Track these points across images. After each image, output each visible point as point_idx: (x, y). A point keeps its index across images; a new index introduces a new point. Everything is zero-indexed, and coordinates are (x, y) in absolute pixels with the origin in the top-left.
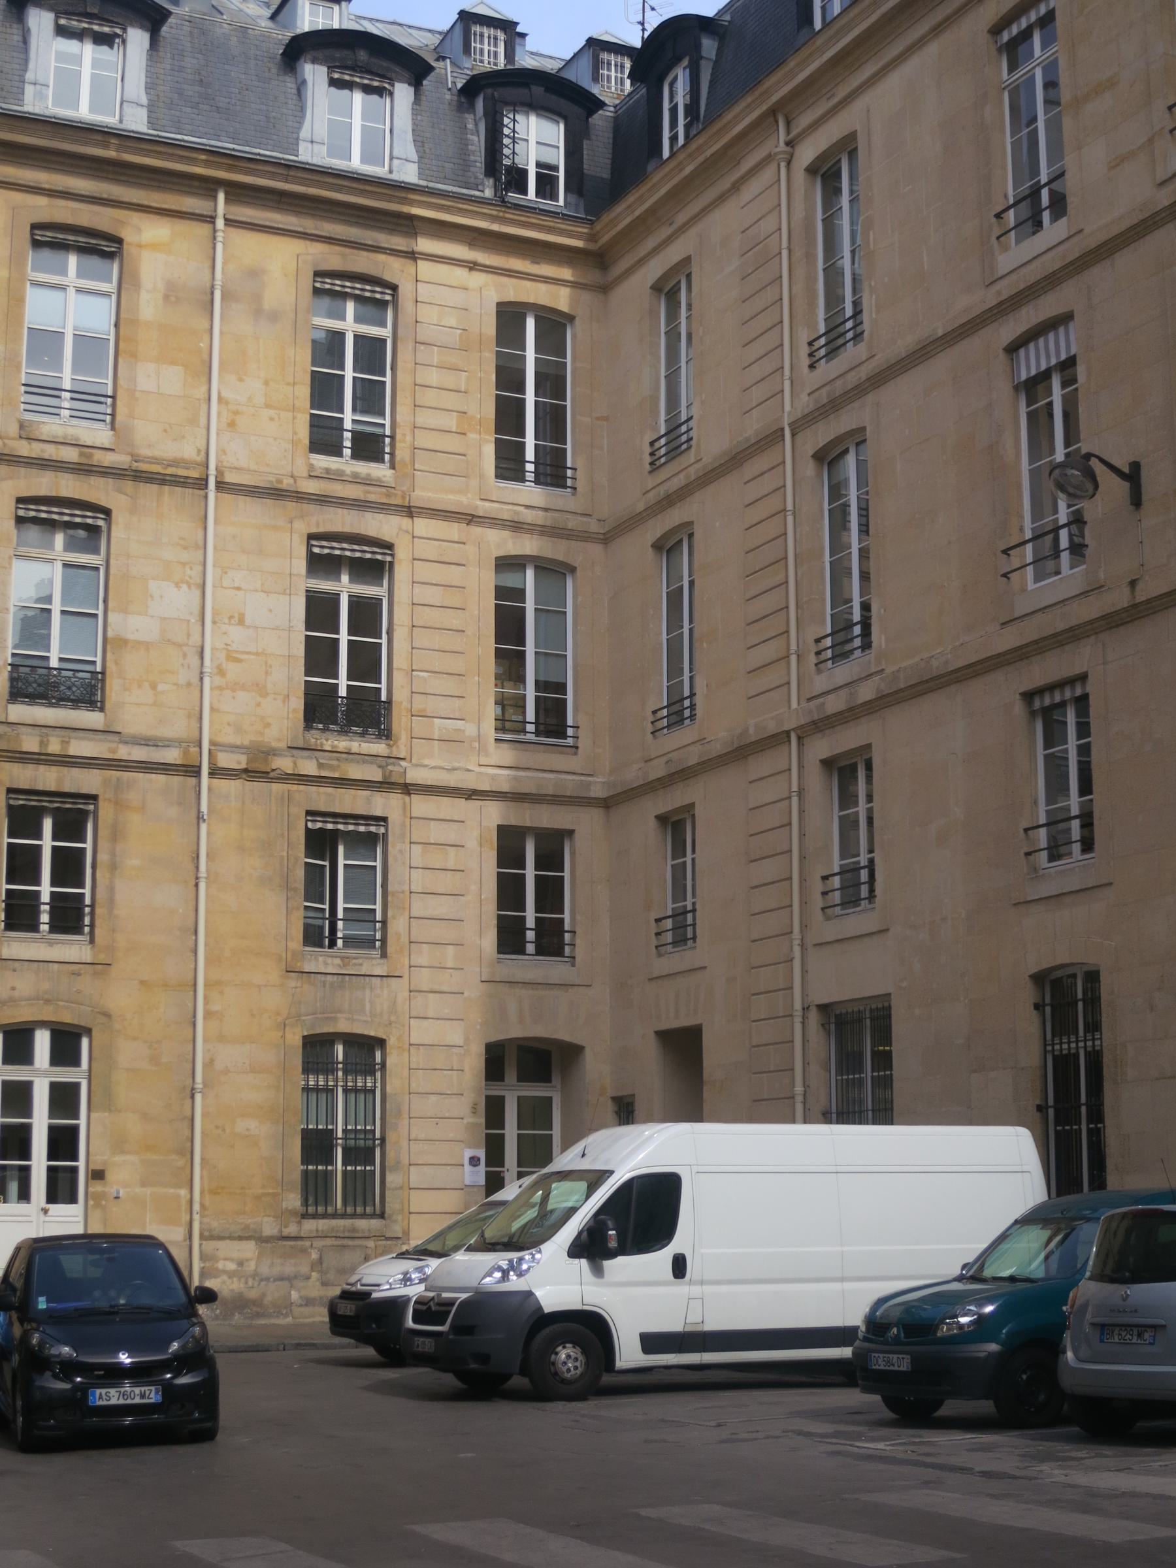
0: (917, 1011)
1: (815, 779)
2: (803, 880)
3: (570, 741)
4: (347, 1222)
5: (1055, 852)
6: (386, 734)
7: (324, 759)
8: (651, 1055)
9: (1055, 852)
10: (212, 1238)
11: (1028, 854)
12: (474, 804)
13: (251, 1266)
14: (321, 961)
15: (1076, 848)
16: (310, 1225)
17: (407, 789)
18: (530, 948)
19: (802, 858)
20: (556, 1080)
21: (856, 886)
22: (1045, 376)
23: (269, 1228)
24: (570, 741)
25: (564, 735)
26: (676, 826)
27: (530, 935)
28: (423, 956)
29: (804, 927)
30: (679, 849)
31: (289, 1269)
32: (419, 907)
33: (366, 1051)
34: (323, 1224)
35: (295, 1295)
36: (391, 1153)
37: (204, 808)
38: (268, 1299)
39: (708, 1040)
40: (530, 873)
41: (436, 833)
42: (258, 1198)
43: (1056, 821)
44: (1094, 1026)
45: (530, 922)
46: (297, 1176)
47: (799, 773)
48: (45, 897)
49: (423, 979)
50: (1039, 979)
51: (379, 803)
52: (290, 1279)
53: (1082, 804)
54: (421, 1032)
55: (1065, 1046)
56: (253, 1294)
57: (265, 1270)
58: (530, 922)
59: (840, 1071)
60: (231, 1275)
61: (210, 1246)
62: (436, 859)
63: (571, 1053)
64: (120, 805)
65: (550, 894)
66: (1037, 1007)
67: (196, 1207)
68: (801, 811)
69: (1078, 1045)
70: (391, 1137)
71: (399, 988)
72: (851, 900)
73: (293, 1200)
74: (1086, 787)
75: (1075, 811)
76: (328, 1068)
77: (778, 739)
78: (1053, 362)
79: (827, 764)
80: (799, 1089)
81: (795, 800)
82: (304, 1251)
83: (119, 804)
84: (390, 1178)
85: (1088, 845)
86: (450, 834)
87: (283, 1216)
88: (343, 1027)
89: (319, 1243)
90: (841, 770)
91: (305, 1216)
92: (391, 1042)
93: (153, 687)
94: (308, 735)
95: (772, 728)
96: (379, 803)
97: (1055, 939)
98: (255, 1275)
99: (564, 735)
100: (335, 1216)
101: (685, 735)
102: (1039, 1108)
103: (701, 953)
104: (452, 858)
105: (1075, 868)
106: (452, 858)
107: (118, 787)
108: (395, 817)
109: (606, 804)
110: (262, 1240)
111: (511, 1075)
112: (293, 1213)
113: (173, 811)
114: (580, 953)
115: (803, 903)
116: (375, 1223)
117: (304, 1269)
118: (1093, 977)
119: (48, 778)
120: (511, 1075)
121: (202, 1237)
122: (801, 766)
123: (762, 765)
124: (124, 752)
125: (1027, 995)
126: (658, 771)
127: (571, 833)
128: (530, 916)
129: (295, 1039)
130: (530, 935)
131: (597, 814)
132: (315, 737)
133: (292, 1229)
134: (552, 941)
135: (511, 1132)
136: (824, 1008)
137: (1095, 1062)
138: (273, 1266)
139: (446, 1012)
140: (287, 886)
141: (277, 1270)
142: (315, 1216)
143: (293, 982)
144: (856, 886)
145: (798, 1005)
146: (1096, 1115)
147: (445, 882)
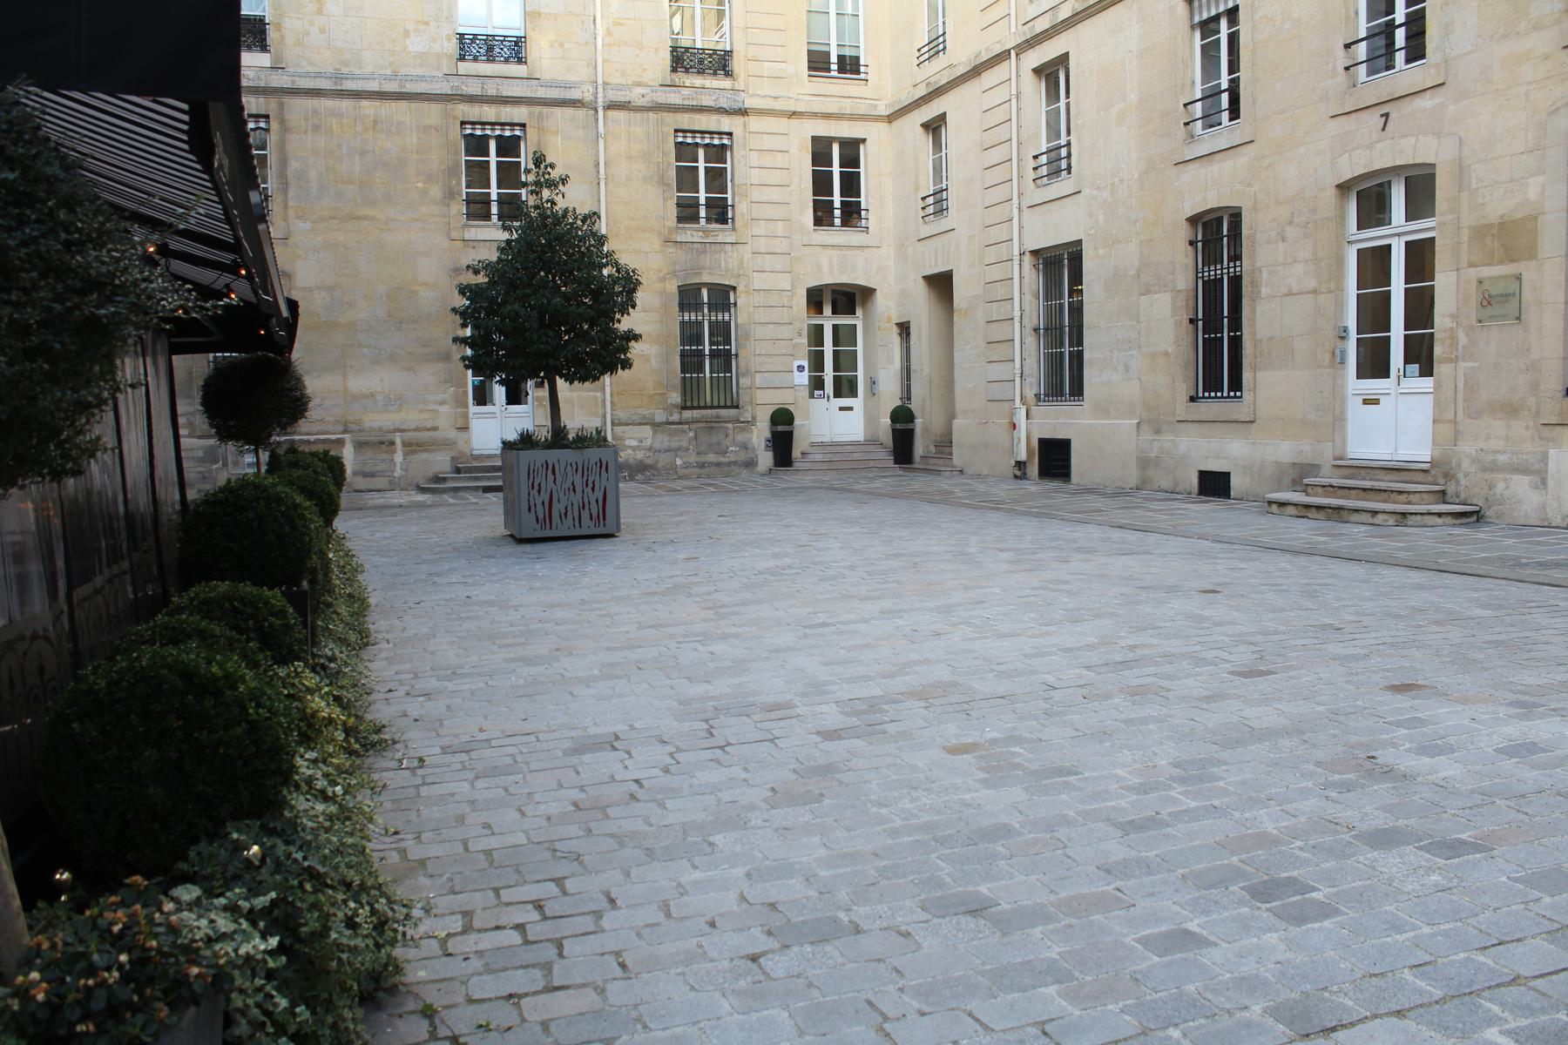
0: (1101, 251)
1: (1029, 79)
2: (1019, 160)
3: (862, 76)
4: (714, 411)
5: (1210, 120)
6: (728, 74)
7: (685, 92)
8: (921, 291)
9: (1210, 120)
10: (620, 424)
11: (1186, 124)
12: (794, 122)
13: (648, 442)
14: (690, 234)
15: (1225, 116)
16: (687, 414)
17: (743, 112)
18: (837, 221)
19: (1019, 144)
20: (859, 312)
21: (1056, 163)
22: (1216, 19)
23: (660, 416)
24: (862, 76)
25: (858, 72)
26: (934, 127)
27: (837, 213)
28: (760, 229)
29: (1020, 194)
30: (937, 145)
31: (674, 444)
32: (756, 194)
33: (722, 297)
34: (696, 413)
35: (679, 462)
36: (742, 364)
37: (601, 129)
38: (660, 465)
39: (957, 281)
40: (836, 170)
41: (768, 142)
42: (651, 397)
43: (1212, 95)
44: (1236, 257)
45: (837, 204)
46: (677, 381)
47: (1018, 82)
48: (494, 197)
49: (762, 245)
50: (1193, 221)
51: (725, 123)
52: (676, 451)
53: (1231, 81)
54: (759, 281)
55: (1211, 273)
56: (649, 462)
57: (657, 445)
58: (837, 204)
59: (1046, 299)
60: (634, 449)
61: (618, 429)
62: (768, 161)
63: (867, 293)
64: (541, 129)
65: (851, 184)
66: (1191, 243)
67: (608, 404)
68: (1019, 109)
69: (1224, 271)
70: (742, 354)
71: (745, 251)
72: (1055, 173)
73: (675, 397)
74: (1234, 66)
75: (1225, 86)
76: (697, 307)
77: (1003, 56)
78: (1222, 9)
79: (1037, 71)
80: (1017, 313)
81: (1014, 101)
82: (683, 431)
83: (540, 129)
84: (742, 381)
85: (1235, 112)
86: (778, 143)
87: (669, 409)
88: (706, 278)
89: (694, 426)
90: (1048, 77)
91: (684, 408)
92: (740, 288)
93: (561, 45)
94: (674, 76)
95: (998, 49)
96: (725, 123)
97: (1208, 189)
98: (650, 449)
99: (858, 72)
100: (706, 407)
101: (941, 62)
102: (1191, 321)
103: (951, 220)
104: (779, 160)
105: (1227, 133)
106: (779, 160)
107: (540, 117)
108: (737, 132)
109: (891, 118)
110: (655, 426)
111: (827, 310)
112: (675, 406)
113: (580, 133)
114: (872, 224)
115: (1020, 177)
116: (732, 412)
117: (685, 444)
118: (1236, 217)
119: (489, 113)
120: (827, 310)
121: (613, 424)
122: (1018, 76)
123: (990, 78)
124: (541, 93)
125: (1184, 233)
126: (922, 91)
127: (864, 141)
128: (837, 199)
129: (672, 287)
130: (837, 213)
131: (883, 126)
132: (681, 77)
133: (675, 417)
134: (852, 214)
135: (828, 348)
136: (1035, 253)
137: (1236, 282)
138: (662, 441)
139: (778, 267)
140: (662, 182)
141: (666, 445)
142: (692, 408)
143: (671, 249)
144: (1056, 163)
145: (1016, 252)
146: (1236, 324)
147: (776, 177)
